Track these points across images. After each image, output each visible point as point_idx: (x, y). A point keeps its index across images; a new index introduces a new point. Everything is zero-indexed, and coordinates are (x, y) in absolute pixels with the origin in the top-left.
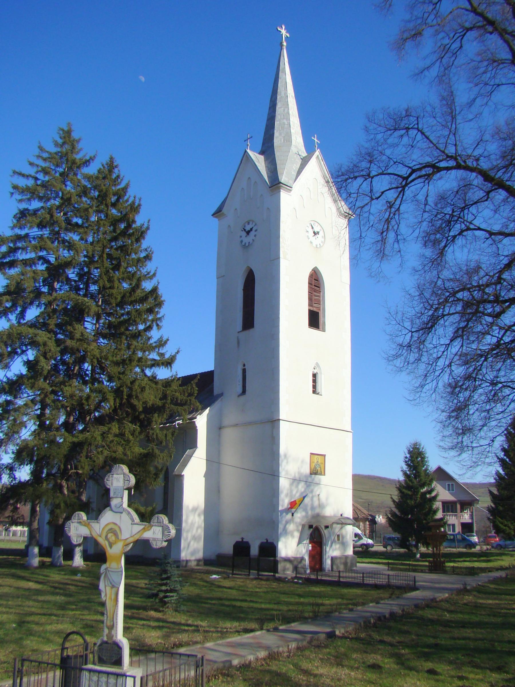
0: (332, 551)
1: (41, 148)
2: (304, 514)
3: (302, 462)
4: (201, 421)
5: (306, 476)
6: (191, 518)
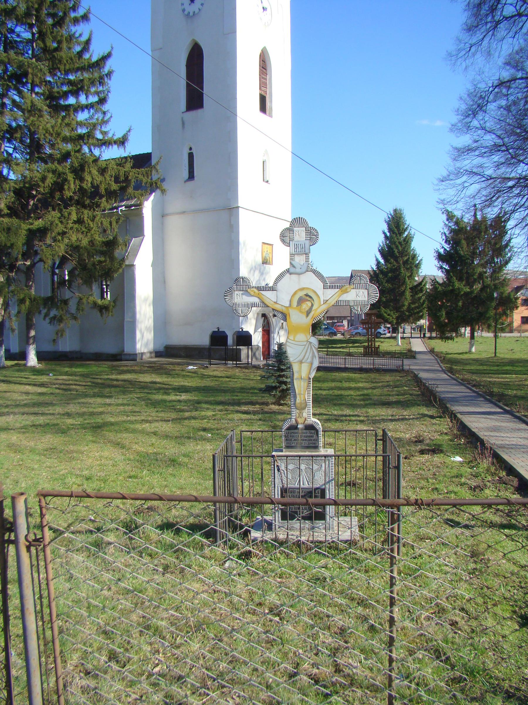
4: (148, 208)
5: (259, 265)
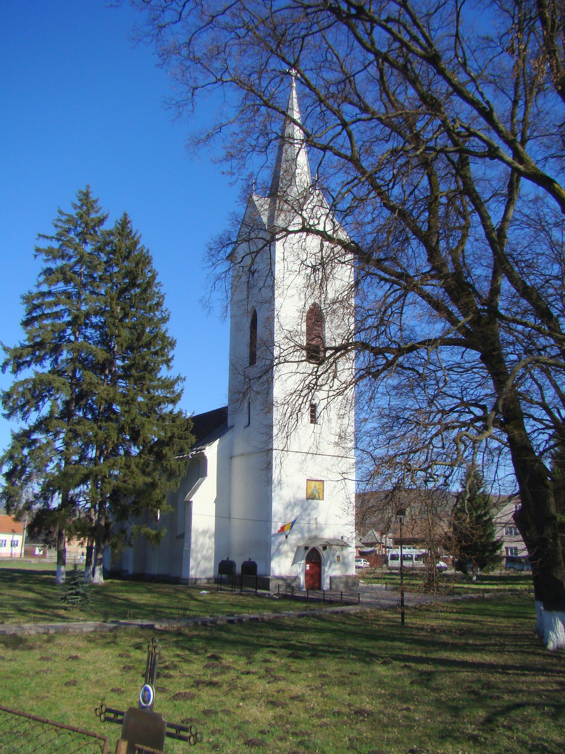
0: (331, 571)
1: (60, 212)
2: (299, 536)
3: (298, 487)
4: (211, 452)
5: (302, 501)
6: (201, 540)
